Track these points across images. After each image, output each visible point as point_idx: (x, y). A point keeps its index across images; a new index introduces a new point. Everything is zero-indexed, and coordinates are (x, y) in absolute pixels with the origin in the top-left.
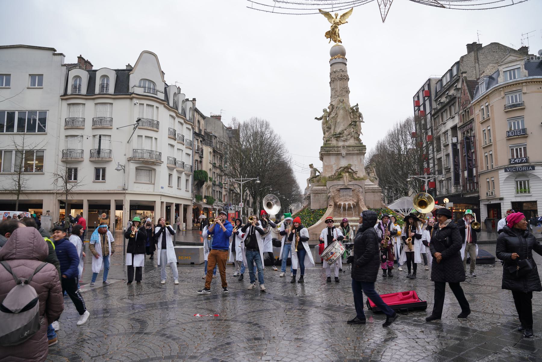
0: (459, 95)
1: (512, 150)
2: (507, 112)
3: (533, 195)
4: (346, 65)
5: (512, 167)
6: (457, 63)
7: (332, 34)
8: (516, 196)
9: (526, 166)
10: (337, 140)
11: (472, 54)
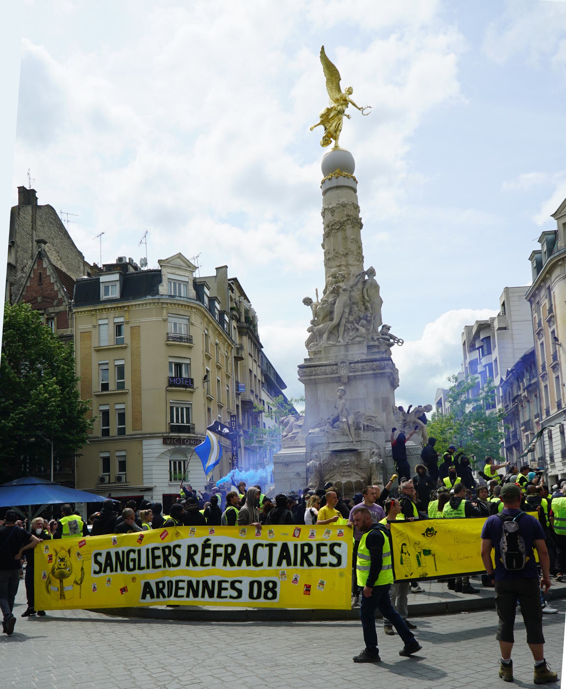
1: (172, 408)
11: (29, 208)
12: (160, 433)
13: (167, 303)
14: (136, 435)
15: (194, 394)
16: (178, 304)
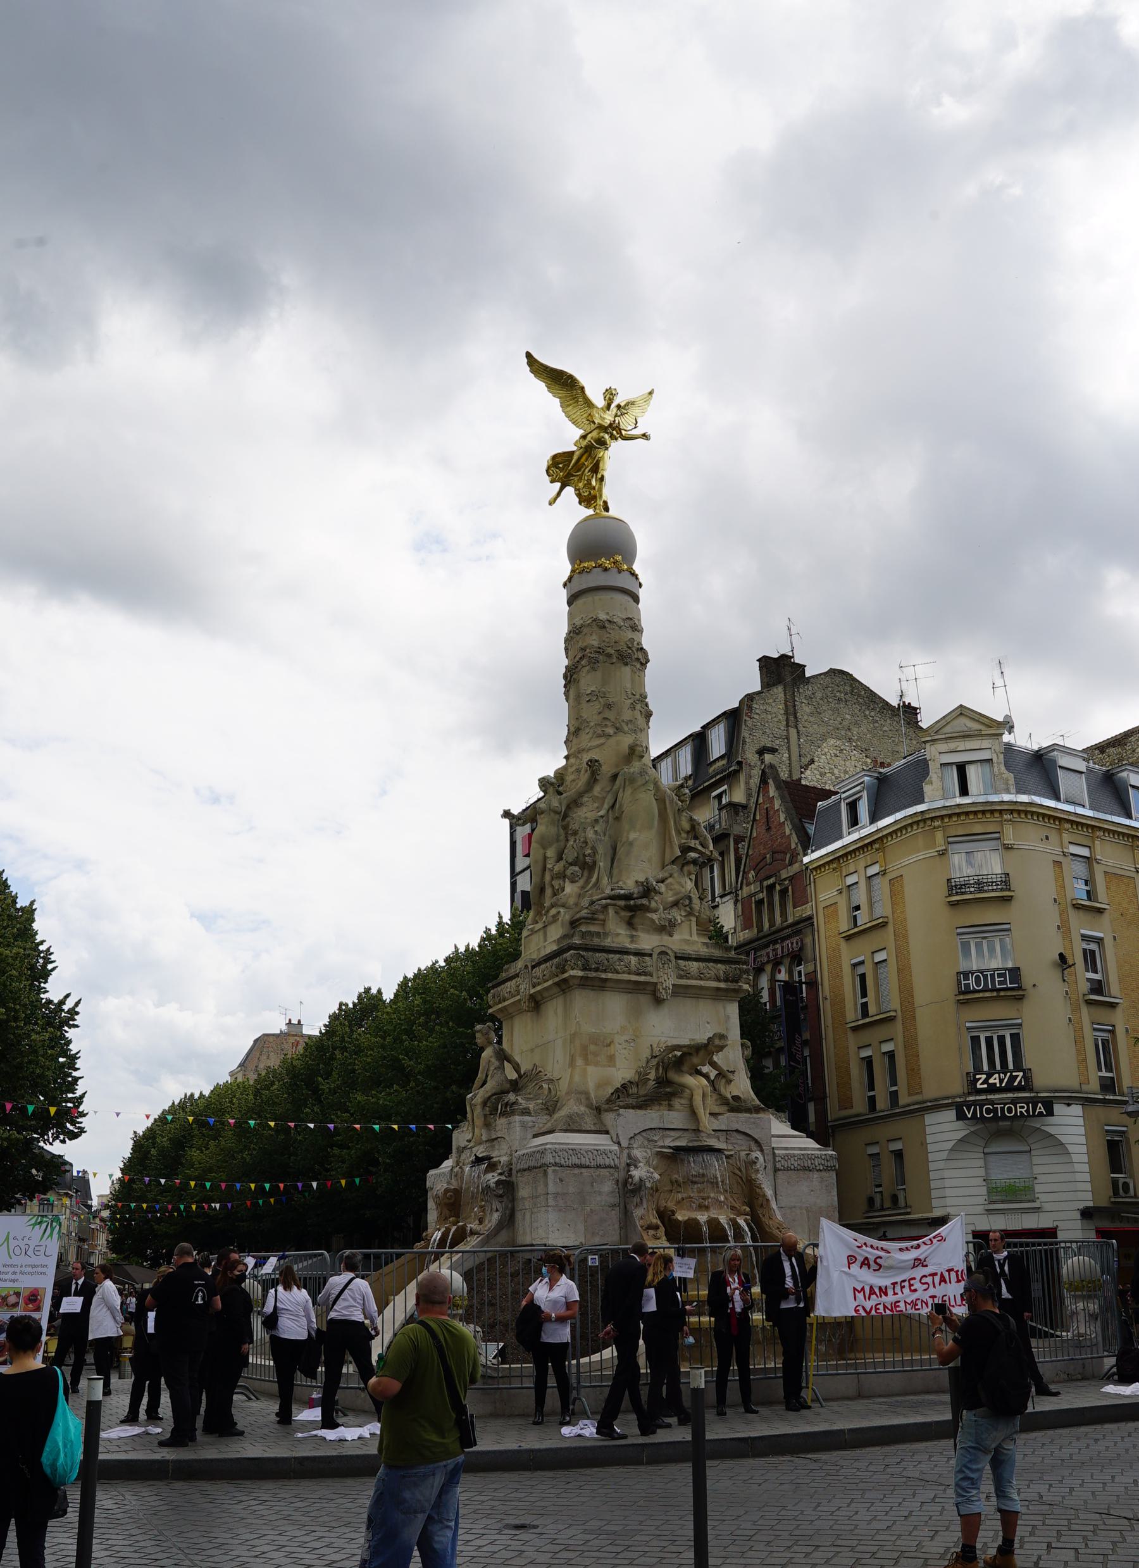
0: (737, 830)
1: (975, 1040)
2: (954, 905)
3: (1047, 1207)
4: (636, 600)
5: (981, 1104)
6: (733, 718)
7: (576, 470)
8: (989, 1212)
9: (1026, 1100)
10: (630, 924)
11: (778, 691)
12: (948, 1098)
14: (909, 1105)
15: (1025, 1001)
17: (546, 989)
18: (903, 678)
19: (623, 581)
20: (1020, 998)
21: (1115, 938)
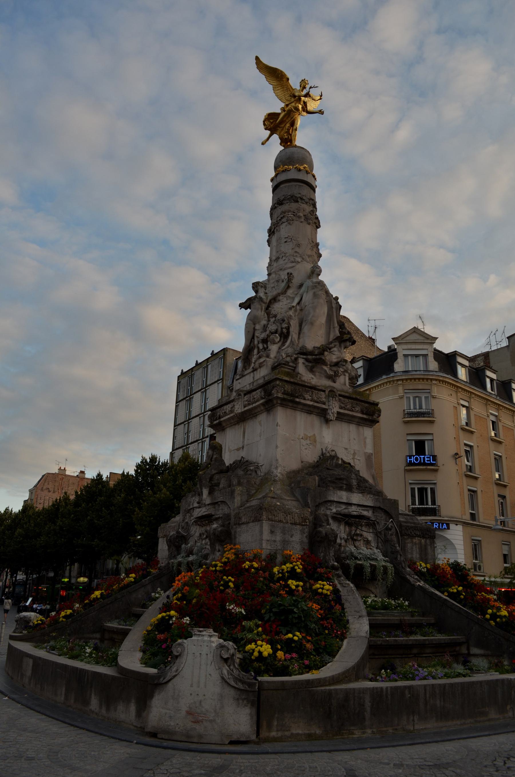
13: (402, 380)
16: (415, 379)
17: (258, 406)
18: (370, 325)
19: (309, 179)
20: (436, 470)
21: (478, 446)
